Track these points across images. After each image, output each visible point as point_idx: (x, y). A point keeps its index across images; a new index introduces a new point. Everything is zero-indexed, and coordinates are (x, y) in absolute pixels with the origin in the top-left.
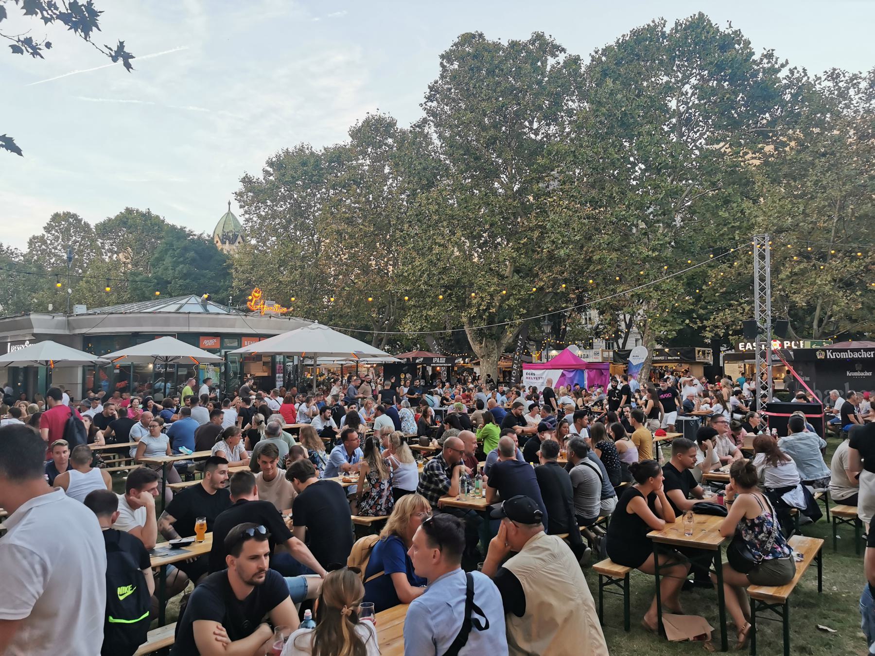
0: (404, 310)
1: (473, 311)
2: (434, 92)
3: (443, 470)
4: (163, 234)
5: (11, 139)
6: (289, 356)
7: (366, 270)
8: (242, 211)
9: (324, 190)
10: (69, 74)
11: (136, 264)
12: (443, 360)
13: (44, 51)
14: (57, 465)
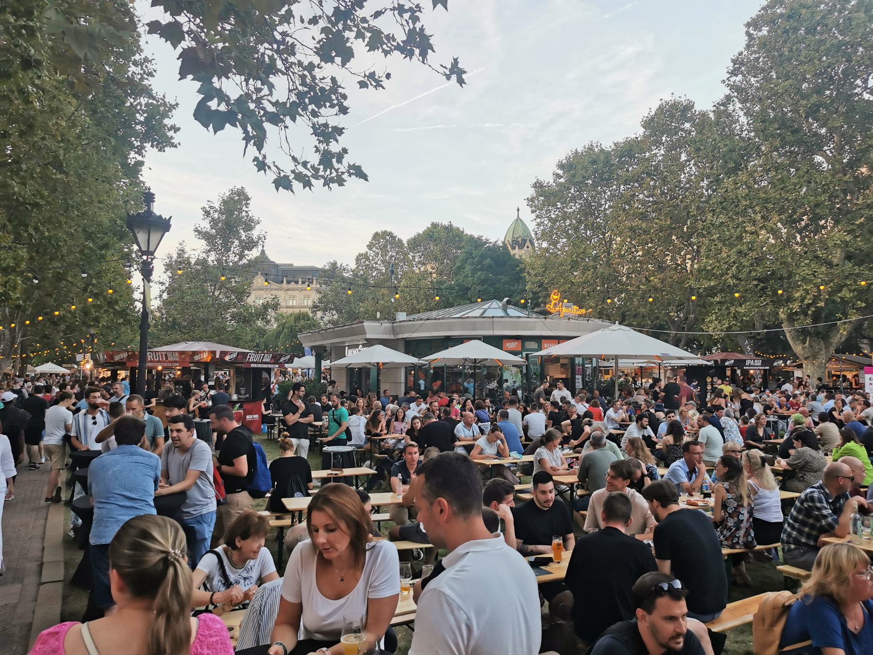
0: (704, 307)
1: (795, 307)
2: (738, 65)
3: (828, 502)
4: (463, 244)
5: (359, 167)
6: (589, 358)
7: (661, 268)
8: (534, 216)
9: (614, 187)
10: (387, 110)
11: (440, 274)
12: (758, 362)
13: (385, 82)
14: (408, 465)
